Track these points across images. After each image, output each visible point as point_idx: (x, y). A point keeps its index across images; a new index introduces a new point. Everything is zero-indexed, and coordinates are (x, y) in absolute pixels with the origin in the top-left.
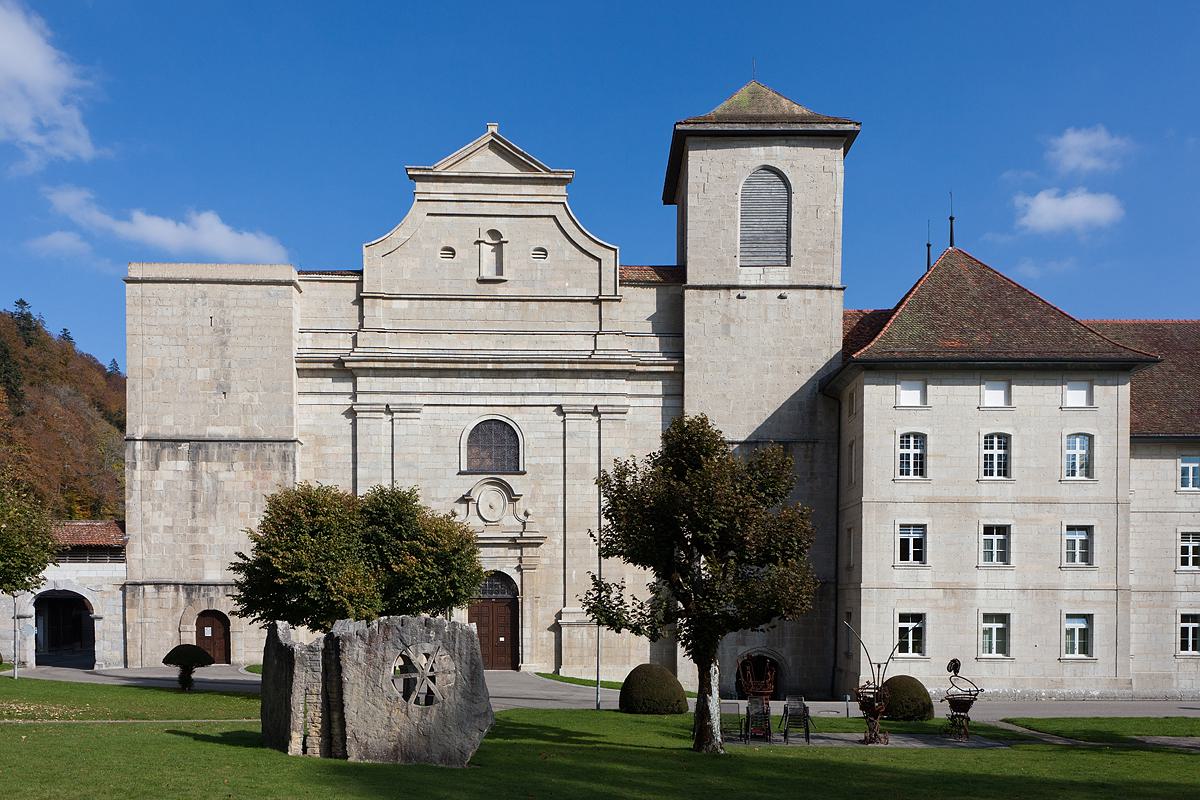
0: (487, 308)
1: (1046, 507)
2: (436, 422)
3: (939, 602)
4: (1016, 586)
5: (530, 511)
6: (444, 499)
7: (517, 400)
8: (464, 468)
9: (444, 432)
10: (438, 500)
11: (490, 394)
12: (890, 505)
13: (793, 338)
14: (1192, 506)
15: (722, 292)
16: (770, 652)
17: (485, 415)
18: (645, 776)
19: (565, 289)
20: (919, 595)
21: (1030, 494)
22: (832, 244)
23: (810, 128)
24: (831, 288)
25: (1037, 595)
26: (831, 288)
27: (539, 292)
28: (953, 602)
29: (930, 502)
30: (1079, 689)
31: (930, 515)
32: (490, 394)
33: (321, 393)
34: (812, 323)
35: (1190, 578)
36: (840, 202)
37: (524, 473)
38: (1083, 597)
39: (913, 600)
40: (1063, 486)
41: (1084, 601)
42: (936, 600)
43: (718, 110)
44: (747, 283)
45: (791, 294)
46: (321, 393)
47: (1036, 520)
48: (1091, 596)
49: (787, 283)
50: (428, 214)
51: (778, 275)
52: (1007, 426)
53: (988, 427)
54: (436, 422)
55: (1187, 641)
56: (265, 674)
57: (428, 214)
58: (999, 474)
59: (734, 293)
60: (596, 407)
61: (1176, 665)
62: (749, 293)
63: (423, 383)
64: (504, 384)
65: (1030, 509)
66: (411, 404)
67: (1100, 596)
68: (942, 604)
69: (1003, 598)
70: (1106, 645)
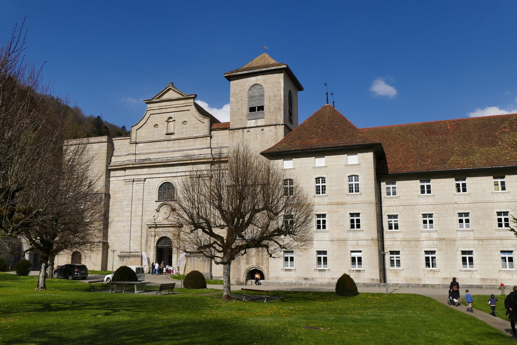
1: (340, 206)
2: (149, 184)
4: (330, 239)
5: (154, 215)
7: (175, 175)
8: (157, 200)
9: (151, 187)
10: (149, 211)
11: (166, 173)
13: (266, 144)
14: (426, 202)
15: (241, 130)
16: (258, 267)
17: (164, 180)
18: (136, 309)
19: (193, 134)
21: (334, 201)
22: (280, 109)
23: (269, 69)
24: (279, 125)
25: (338, 242)
26: (279, 125)
27: (184, 136)
30: (319, 281)
32: (166, 173)
33: (116, 177)
35: (427, 234)
36: (282, 93)
38: (357, 243)
40: (348, 197)
41: (357, 245)
43: (246, 66)
44: (250, 126)
45: (266, 129)
46: (116, 177)
49: (264, 125)
50: (189, 110)
51: (261, 122)
54: (149, 184)
55: (429, 263)
57: (189, 110)
58: (356, 192)
59: (245, 130)
61: (423, 274)
62: (252, 130)
63: (145, 171)
64: (171, 169)
65: (334, 207)
66: (140, 179)
69: (324, 244)
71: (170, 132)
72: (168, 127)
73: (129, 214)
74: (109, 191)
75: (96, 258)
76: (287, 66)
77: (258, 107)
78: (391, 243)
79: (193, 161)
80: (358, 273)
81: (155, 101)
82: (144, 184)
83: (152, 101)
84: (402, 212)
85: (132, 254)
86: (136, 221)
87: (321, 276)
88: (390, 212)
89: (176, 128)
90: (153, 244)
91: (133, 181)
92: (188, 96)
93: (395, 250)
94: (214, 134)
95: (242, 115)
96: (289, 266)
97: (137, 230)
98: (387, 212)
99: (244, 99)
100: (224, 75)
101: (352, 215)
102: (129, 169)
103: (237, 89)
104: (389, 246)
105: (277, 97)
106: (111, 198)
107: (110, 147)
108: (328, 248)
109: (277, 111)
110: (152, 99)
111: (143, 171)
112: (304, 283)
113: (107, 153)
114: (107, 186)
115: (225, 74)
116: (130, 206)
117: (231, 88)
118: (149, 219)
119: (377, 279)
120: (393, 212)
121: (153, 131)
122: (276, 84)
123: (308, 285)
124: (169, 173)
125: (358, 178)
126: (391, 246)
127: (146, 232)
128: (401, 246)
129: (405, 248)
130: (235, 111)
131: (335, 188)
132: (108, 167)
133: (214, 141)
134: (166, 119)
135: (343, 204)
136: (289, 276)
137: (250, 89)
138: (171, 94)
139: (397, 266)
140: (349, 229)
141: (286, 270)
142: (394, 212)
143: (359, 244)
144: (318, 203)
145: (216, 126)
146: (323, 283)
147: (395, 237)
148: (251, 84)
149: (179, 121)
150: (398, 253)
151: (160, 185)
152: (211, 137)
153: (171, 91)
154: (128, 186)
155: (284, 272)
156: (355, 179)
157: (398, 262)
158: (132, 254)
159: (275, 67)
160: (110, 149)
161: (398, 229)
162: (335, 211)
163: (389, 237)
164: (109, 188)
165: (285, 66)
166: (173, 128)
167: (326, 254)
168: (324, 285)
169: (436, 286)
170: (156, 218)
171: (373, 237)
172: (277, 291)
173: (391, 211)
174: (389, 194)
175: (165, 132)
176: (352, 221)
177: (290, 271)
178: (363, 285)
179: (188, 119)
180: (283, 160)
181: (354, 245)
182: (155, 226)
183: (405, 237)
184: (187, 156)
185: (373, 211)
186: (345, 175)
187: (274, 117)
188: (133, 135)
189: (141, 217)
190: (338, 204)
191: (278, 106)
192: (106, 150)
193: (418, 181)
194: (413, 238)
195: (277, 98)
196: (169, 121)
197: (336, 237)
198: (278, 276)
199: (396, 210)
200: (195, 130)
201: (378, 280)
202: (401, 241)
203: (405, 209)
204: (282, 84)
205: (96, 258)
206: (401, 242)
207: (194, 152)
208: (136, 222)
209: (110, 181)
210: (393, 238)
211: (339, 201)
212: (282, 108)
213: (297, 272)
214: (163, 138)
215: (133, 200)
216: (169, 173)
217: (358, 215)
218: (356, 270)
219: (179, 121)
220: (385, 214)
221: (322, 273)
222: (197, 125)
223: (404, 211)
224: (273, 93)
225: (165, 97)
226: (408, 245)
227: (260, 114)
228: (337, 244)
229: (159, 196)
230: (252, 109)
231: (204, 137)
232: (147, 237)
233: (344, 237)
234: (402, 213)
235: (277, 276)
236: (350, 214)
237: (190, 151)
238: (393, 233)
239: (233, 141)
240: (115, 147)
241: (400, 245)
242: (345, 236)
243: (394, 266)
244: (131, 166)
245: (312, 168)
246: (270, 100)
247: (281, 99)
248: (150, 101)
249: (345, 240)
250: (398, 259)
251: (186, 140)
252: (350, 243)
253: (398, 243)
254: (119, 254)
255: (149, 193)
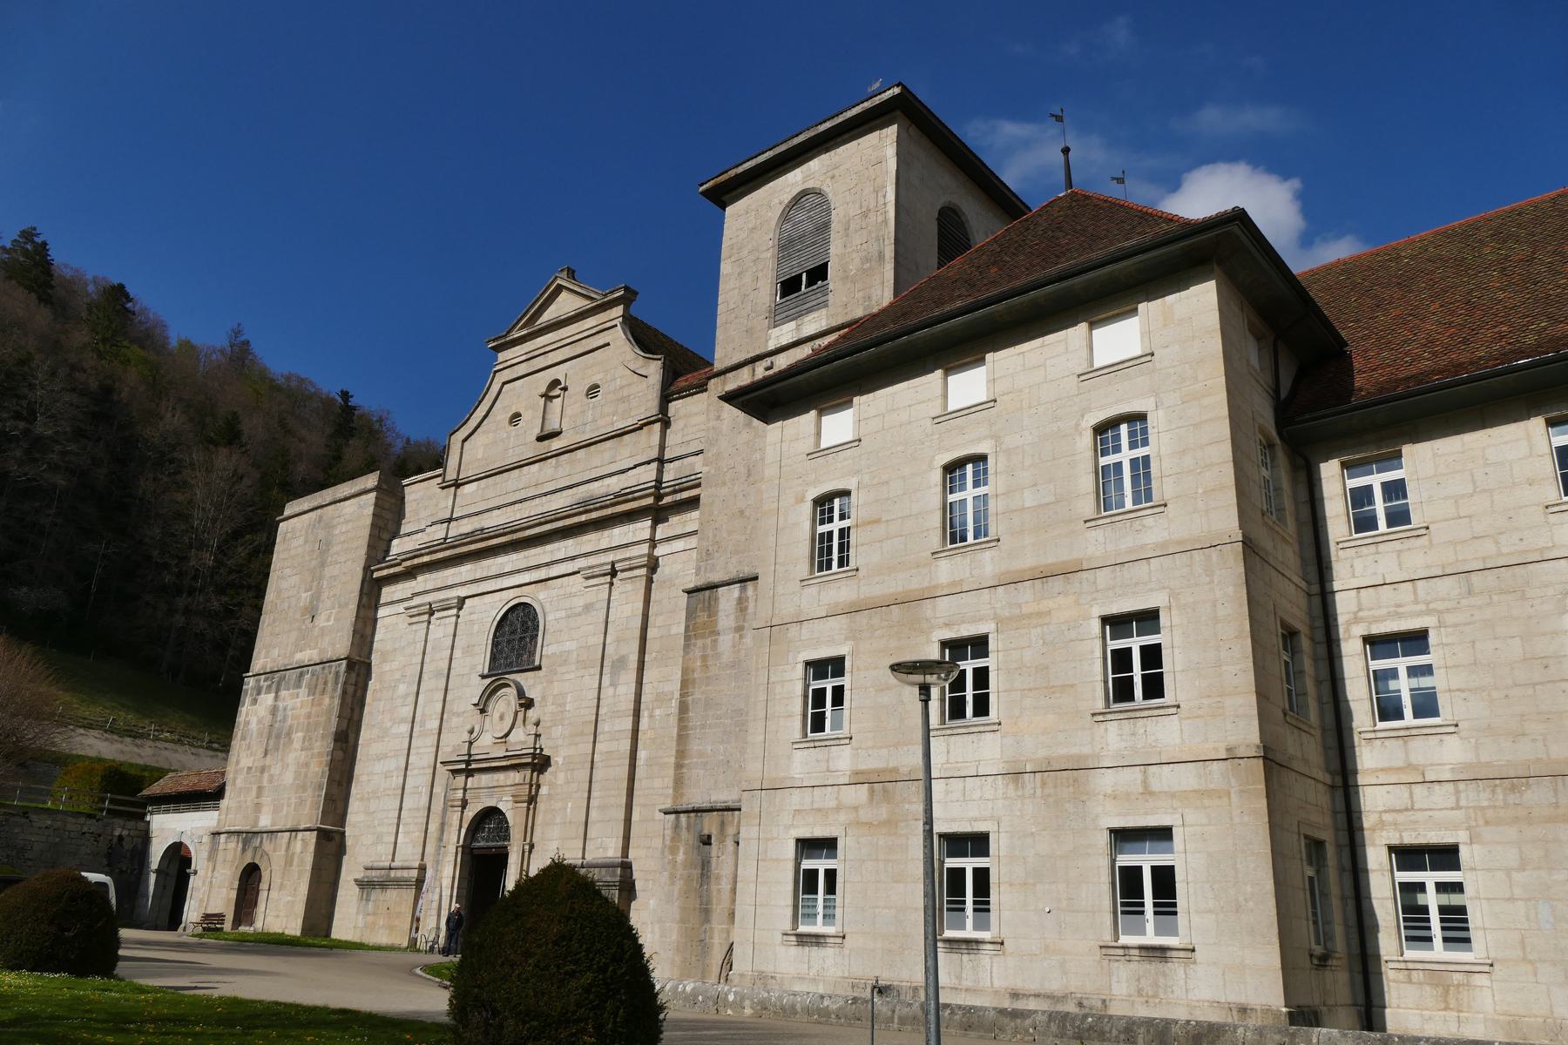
0: (541, 470)
1: (1057, 584)
3: (861, 812)
4: (1001, 768)
6: (463, 713)
8: (486, 672)
12: (794, 629)
20: (827, 798)
22: (881, 256)
25: (1044, 784)
28: (883, 812)
29: (854, 610)
31: (853, 635)
34: (1061, 386)
37: (539, 668)
38: (1145, 782)
39: (819, 810)
41: (1147, 792)
42: (856, 809)
47: (1039, 614)
48: (1164, 778)
50: (608, 344)
52: (980, 440)
53: (948, 450)
56: (116, 943)
57: (608, 344)
60: (613, 564)
63: (466, 571)
65: (1026, 593)
67: (1187, 778)
68: (865, 815)
69: (976, 795)
70: (1210, 911)
71: (549, 428)
72: (548, 416)
73: (405, 728)
74: (370, 653)
75: (295, 890)
76: (904, 87)
77: (808, 272)
78: (1399, 796)
79: (594, 515)
80: (1153, 967)
81: (515, 336)
82: (458, 617)
83: (507, 339)
84: (1448, 611)
85: (393, 874)
86: (421, 751)
87: (959, 978)
88: (1377, 620)
89: (568, 411)
90: (454, 838)
91: (431, 613)
92: (605, 295)
93: (1422, 840)
94: (677, 411)
95: (754, 315)
96: (820, 918)
97: (418, 787)
98: (1357, 620)
99: (764, 255)
100: (701, 189)
101: (1117, 624)
102: (423, 572)
103: (741, 229)
104: (1386, 817)
105: (870, 215)
106: (373, 675)
107: (387, 505)
108: (992, 818)
109: (870, 268)
110: (508, 332)
111: (461, 573)
112: (731, 998)
113: (373, 525)
114: (362, 636)
115: (701, 185)
116: (412, 699)
117: (726, 232)
118: (454, 744)
119: (1267, 1011)
120: (1398, 616)
121: (505, 435)
122: (871, 169)
123: (748, 1011)
124: (528, 569)
125: (1144, 431)
126: (1401, 818)
127: (443, 794)
128: (1459, 814)
129: (1487, 823)
130: (732, 306)
131: (1029, 499)
132: (373, 572)
133: (673, 437)
134: (543, 390)
135: (1068, 572)
136: (813, 973)
137: (785, 217)
138: (566, 304)
139: (1445, 940)
140: (1100, 705)
141: (804, 940)
142: (1399, 616)
143: (1155, 786)
144: (953, 584)
145: (686, 380)
146: (826, 1003)
147: (1417, 758)
148: (787, 198)
149: (577, 388)
150: (1446, 856)
151: (498, 618)
152: (666, 423)
153: (564, 294)
154: (416, 631)
155: (794, 951)
156: (1132, 434)
157: (1455, 918)
158: (393, 874)
159: (861, 105)
160: (388, 515)
161: (1434, 712)
162: (1030, 616)
163: (1380, 766)
164: (372, 642)
165: (897, 90)
166: (558, 420)
167: (985, 853)
168: (825, 1013)
169: (629, 870)
170: (477, 739)
171: (1232, 740)
172: (269, 1003)
173: (1384, 611)
174: (1365, 523)
175: (537, 431)
176: (1121, 659)
177: (818, 944)
178: (1054, 1027)
179: (600, 376)
180: (821, 413)
181: (1128, 794)
182: (464, 766)
183: (1484, 758)
184: (584, 503)
185: (1230, 590)
186: (1077, 425)
187: (861, 294)
188: (452, 462)
189: (436, 736)
190: (1044, 576)
191: (873, 249)
192: (371, 517)
193: (1537, 424)
194: (1538, 760)
195: (872, 218)
196: (552, 394)
197: (1034, 750)
198: (769, 968)
199: (1416, 602)
200: (621, 407)
201: (1277, 1014)
202: (1462, 786)
203: (1470, 592)
204: (892, 164)
205: (295, 890)
206: (1457, 792)
207: (608, 485)
208: (422, 758)
209: (375, 620)
210: (1410, 767)
211: (1050, 561)
212: (889, 252)
213: (847, 952)
214: (529, 454)
215: (425, 676)
216: (528, 569)
217: (1148, 619)
218: (1141, 948)
219: (577, 388)
220: (1347, 630)
221: (965, 957)
222: (625, 392)
223: (1464, 602)
224: (857, 206)
225: (548, 315)
226: (1506, 805)
227: (813, 298)
228: (1039, 791)
229: (493, 658)
230: (789, 287)
231: (640, 428)
232: (445, 811)
233: (1075, 750)
234: (1450, 619)
235: (764, 969)
236: (1105, 620)
237: (596, 484)
238: (1407, 735)
239: (718, 418)
240: (408, 508)
241: (1458, 807)
242: (1078, 745)
243: (1430, 939)
244: (426, 559)
245: (929, 422)
246: (847, 236)
247: (885, 222)
248: (503, 341)
249: (1080, 768)
250: (1454, 899)
251: (593, 447)
252: (1105, 781)
253: (1442, 796)
254: (359, 876)
255: (468, 649)
